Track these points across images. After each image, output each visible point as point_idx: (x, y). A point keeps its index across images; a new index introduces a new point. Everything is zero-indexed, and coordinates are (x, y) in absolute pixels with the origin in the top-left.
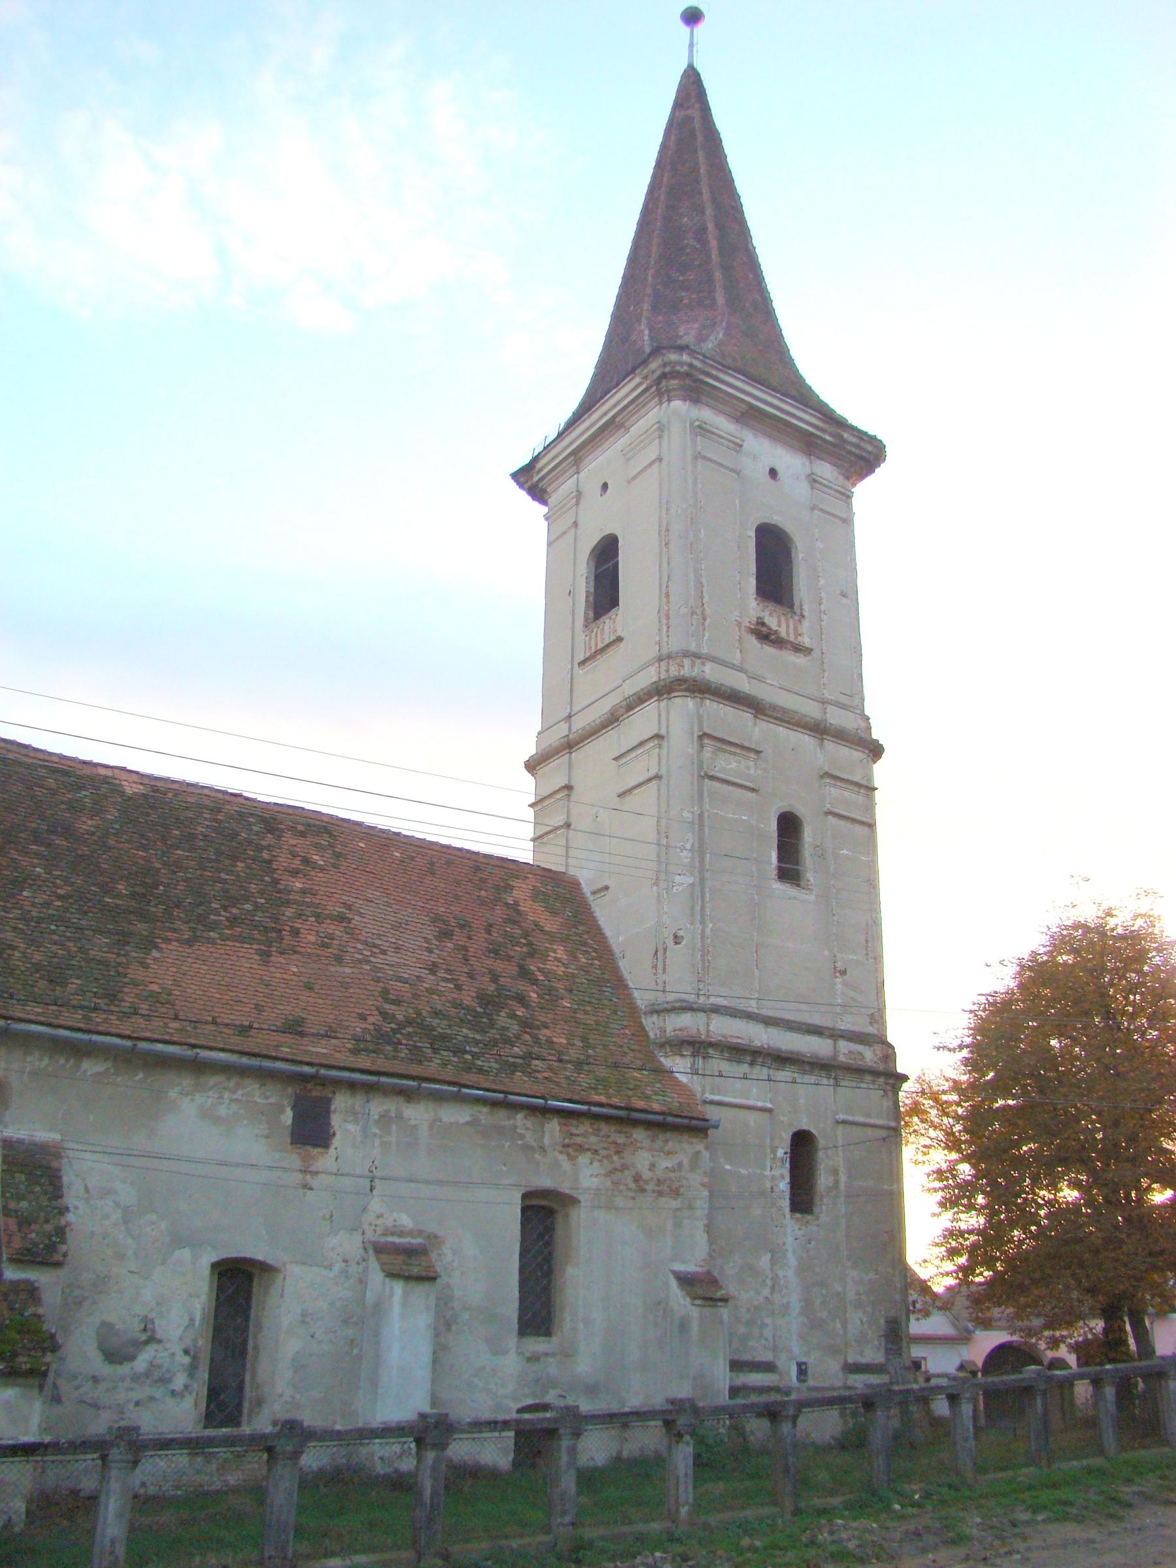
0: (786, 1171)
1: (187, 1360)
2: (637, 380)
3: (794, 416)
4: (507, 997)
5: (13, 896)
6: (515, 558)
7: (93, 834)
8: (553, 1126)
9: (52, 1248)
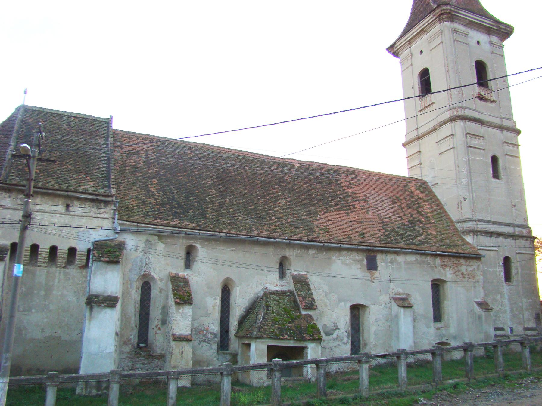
0: (502, 269)
1: (347, 334)
2: (432, 16)
3: (483, 22)
4: (416, 221)
5: (276, 202)
6: (393, 78)
7: (291, 181)
8: (438, 260)
9: (312, 305)
